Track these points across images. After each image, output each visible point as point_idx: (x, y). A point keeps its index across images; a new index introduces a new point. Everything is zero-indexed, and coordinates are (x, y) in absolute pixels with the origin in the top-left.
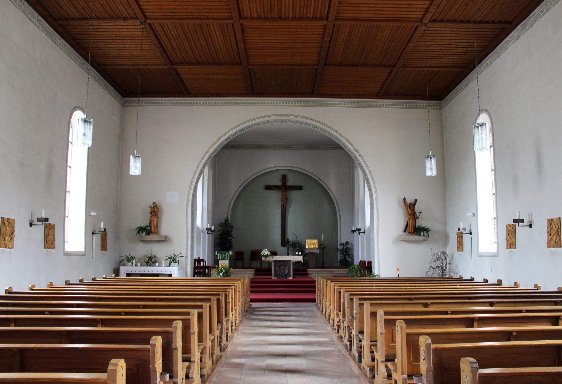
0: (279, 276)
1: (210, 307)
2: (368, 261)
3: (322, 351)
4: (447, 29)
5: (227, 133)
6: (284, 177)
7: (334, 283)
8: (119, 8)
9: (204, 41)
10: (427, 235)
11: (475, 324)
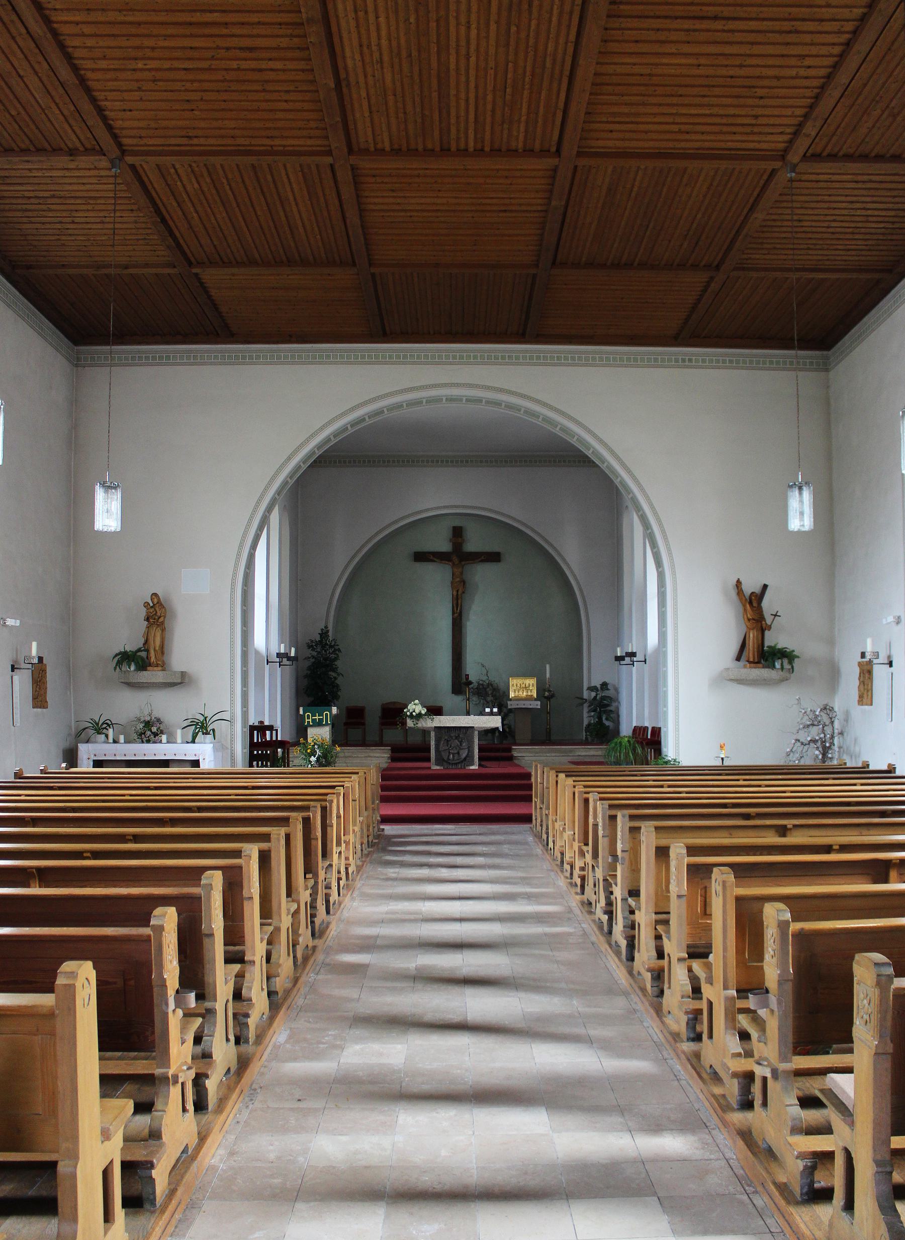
0: (446, 762)
1: (288, 837)
2: (653, 728)
3: (545, 934)
4: (845, 177)
5: (322, 428)
6: (458, 532)
7: (574, 778)
8: (57, 126)
9: (265, 208)
10: (790, 667)
11: (893, 874)
